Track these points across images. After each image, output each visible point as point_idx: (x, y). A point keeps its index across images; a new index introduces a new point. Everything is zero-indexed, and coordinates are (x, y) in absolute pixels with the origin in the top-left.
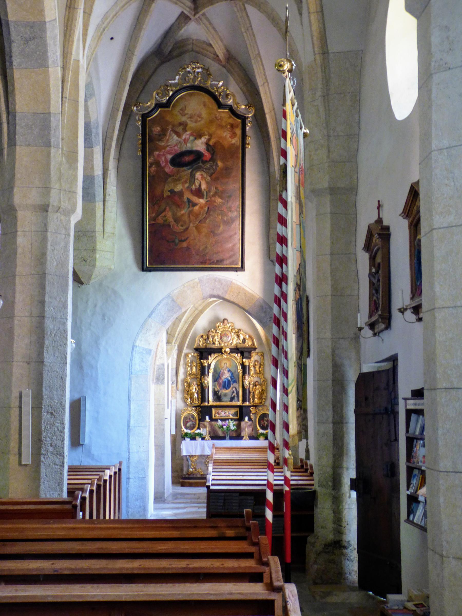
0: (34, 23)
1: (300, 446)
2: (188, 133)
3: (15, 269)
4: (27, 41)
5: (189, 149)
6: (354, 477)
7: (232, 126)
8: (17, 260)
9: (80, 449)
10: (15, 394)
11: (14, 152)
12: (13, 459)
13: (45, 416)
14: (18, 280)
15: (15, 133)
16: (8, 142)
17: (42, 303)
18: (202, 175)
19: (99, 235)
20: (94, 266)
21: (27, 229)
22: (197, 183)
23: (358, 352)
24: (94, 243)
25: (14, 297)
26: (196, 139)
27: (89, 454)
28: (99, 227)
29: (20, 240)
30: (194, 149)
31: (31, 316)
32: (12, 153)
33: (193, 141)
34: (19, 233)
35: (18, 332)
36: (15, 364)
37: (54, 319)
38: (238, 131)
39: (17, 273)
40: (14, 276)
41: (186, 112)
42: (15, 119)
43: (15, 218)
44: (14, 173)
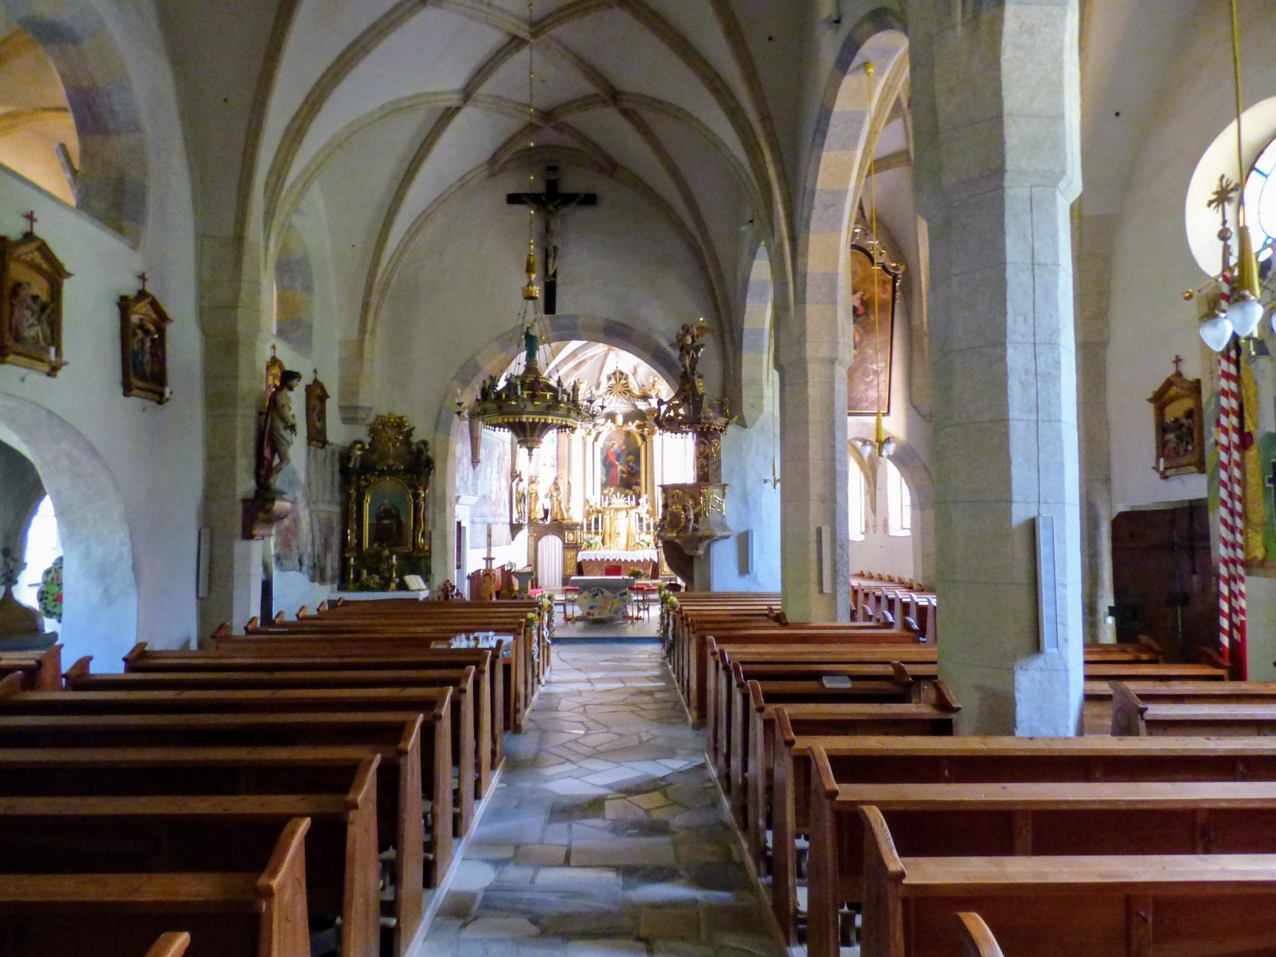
4: (827, 207)
6: (1112, 604)
7: (884, 282)
9: (747, 577)
10: (813, 529)
12: (814, 588)
13: (838, 549)
15: (804, 291)
17: (833, 447)
19: (764, 382)
20: (762, 411)
23: (1109, 491)
24: (761, 391)
27: (756, 581)
28: (765, 377)
29: (810, 390)
31: (824, 459)
35: (812, 473)
38: (889, 287)
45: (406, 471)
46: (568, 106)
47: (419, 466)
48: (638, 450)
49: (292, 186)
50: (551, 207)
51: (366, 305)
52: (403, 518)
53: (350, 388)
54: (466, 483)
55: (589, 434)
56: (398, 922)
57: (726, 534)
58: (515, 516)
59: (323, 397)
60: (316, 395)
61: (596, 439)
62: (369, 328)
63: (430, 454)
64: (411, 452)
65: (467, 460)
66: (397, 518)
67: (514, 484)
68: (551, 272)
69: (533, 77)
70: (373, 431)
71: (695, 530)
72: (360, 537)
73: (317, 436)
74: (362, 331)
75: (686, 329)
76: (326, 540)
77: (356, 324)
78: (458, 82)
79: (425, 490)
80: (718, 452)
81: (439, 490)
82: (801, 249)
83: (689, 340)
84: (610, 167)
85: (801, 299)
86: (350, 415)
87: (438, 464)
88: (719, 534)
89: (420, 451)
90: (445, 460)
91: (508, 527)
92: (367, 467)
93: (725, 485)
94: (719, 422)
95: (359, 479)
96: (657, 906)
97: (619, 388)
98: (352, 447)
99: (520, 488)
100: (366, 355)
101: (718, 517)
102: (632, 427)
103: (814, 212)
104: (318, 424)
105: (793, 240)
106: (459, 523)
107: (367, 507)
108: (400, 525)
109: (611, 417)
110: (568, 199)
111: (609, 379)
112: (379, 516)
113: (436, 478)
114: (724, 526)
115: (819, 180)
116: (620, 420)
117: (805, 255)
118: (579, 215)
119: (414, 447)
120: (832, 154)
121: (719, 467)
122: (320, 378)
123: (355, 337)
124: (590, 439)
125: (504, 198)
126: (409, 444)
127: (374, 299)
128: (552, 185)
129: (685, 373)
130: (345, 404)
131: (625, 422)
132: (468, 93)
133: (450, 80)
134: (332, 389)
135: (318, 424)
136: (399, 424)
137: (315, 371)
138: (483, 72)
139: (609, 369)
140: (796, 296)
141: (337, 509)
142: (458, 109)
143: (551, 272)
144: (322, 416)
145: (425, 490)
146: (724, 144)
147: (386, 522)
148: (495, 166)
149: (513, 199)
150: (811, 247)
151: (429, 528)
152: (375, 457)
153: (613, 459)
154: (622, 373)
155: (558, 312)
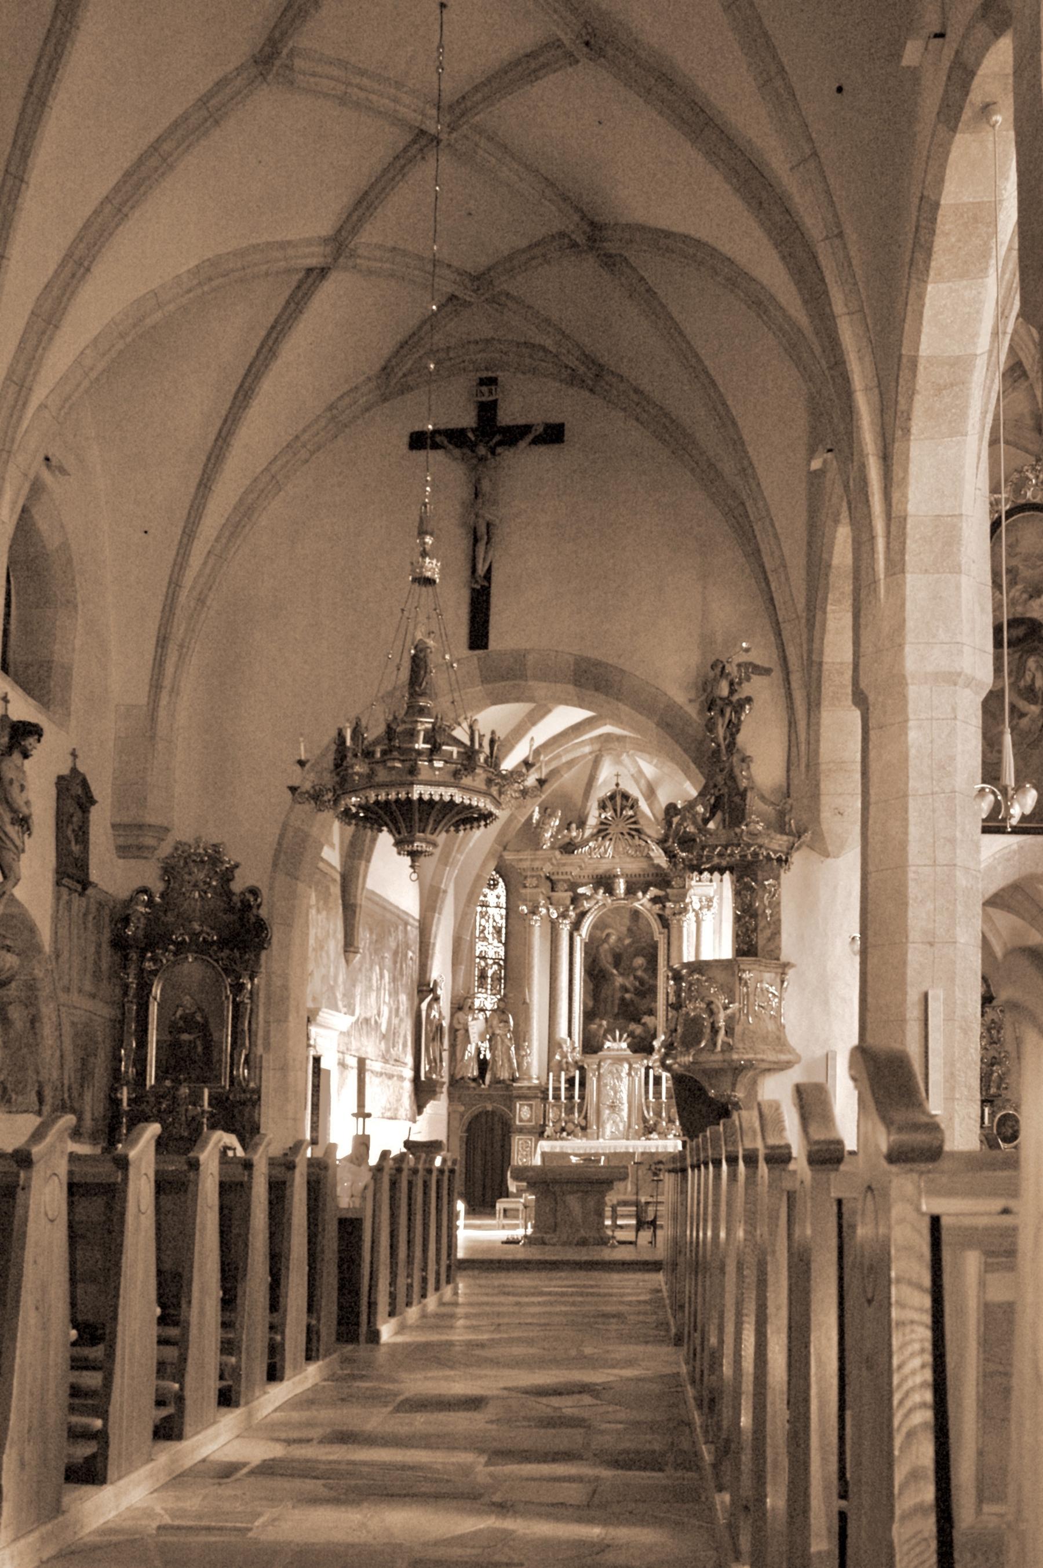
0: (958, 357)
1: (287, 1347)
2: (1020, 587)
3: (907, 784)
4: (939, 390)
5: (1018, 616)
8: (910, 770)
11: (901, 586)
14: (912, 805)
15: (903, 552)
16: (887, 569)
18: (1037, 662)
21: (923, 716)
22: (1028, 678)
25: (906, 834)
26: (1031, 597)
30: (1028, 615)
32: (897, 589)
33: (1026, 602)
34: (911, 724)
36: (910, 945)
37: (967, 869)
39: (910, 792)
40: (906, 796)
41: (1018, 550)
42: (904, 528)
43: (904, 698)
44: (904, 620)
45: (223, 943)
46: (513, 263)
47: (241, 934)
48: (655, 947)
49: (43, 406)
50: (482, 450)
51: (162, 641)
52: (216, 1036)
53: (132, 791)
54: (332, 989)
55: (564, 915)
56: (105, 1425)
57: (783, 1057)
58: (424, 1067)
59: (86, 801)
60: (74, 795)
61: (576, 926)
62: (167, 683)
63: (263, 913)
64: (231, 909)
65: (335, 944)
66: (204, 1030)
67: (424, 1005)
68: (481, 570)
69: (453, 215)
70: (169, 871)
71: (728, 1048)
72: (141, 1062)
73: (72, 871)
74: (156, 686)
75: (719, 668)
76: (84, 1062)
77: (145, 675)
78: (325, 227)
79: (252, 979)
80: (776, 905)
81: (278, 982)
82: (897, 472)
83: (724, 690)
84: (592, 375)
85: (896, 566)
86: (131, 842)
87: (276, 935)
88: (771, 1056)
89: (247, 907)
90: (288, 925)
91: (408, 1086)
92: (155, 940)
93: (786, 965)
94: (778, 842)
95: (142, 958)
96: (546, 1544)
97: (624, 827)
98: (132, 900)
99: (434, 1013)
100: (162, 729)
101: (771, 1026)
102: (643, 902)
103: (918, 398)
104: (75, 848)
105: (886, 458)
106: (317, 1060)
107: (154, 1009)
108: (209, 1045)
109: (605, 882)
110: (514, 435)
111: (603, 806)
112: (171, 1028)
113: (270, 959)
114: (780, 1041)
115: (924, 338)
116: (621, 886)
117: (904, 481)
118: (524, 464)
119: (235, 899)
120: (942, 286)
121: (777, 933)
122: (82, 768)
123: (142, 698)
124: (565, 928)
125: (406, 440)
126: (229, 894)
127: (179, 631)
128: (487, 411)
129: (716, 752)
130: (118, 820)
131: (630, 891)
132: (340, 244)
133: (310, 224)
134: (102, 789)
135: (75, 848)
136: (214, 857)
137: (74, 754)
138: (364, 204)
139: (603, 787)
140: (888, 559)
141: (106, 1012)
142: (323, 272)
143: (481, 570)
144: (82, 835)
145: (252, 979)
146: (772, 298)
147: (185, 1037)
148: (392, 379)
149: (418, 441)
150: (913, 469)
151: (260, 1050)
152: (170, 918)
153: (606, 962)
154: (625, 796)
155: (495, 642)
